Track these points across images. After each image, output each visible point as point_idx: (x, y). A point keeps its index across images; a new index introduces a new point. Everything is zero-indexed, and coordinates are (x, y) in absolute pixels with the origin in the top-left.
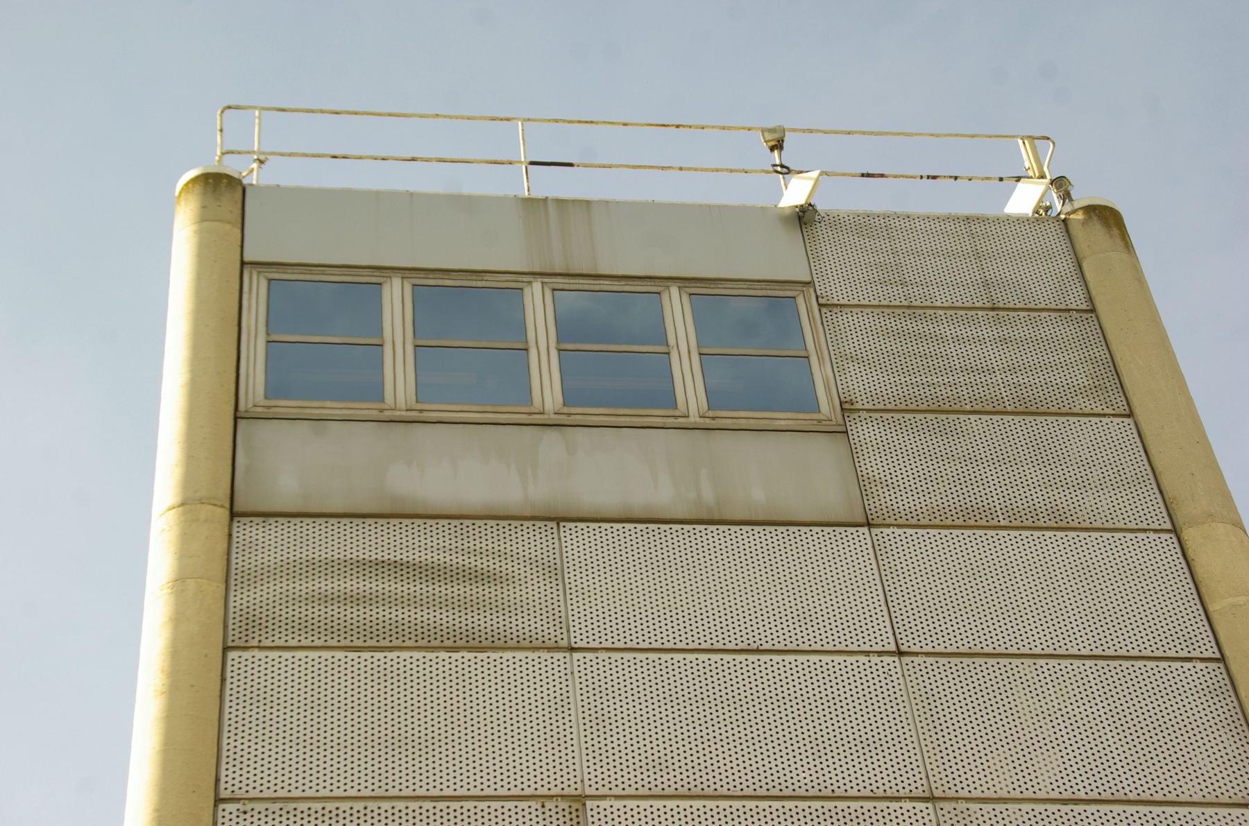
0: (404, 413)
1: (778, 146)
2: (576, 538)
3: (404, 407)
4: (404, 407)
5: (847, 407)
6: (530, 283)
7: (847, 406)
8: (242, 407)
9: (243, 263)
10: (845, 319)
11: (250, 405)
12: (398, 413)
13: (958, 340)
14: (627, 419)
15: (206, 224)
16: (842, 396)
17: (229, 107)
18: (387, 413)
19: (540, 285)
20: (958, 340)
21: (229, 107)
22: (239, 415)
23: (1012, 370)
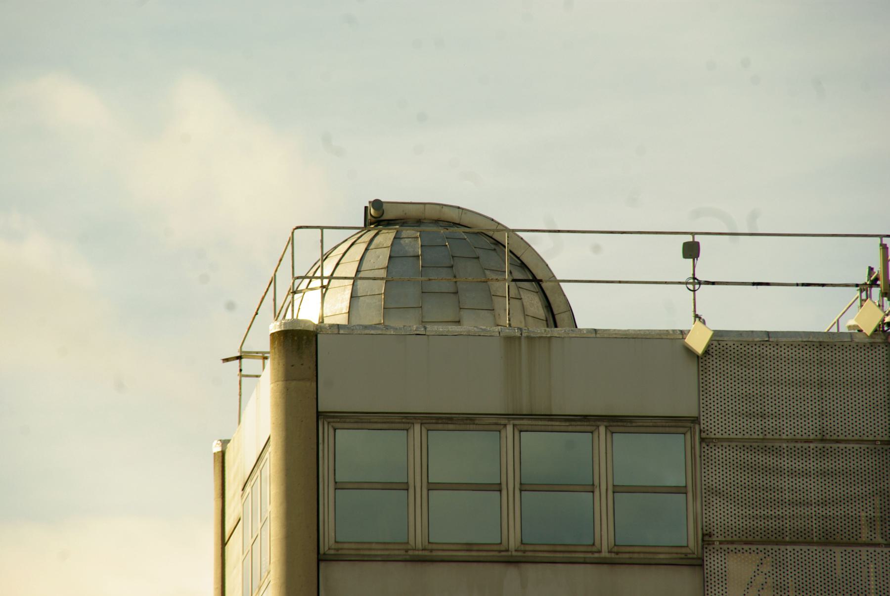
0: (420, 553)
1: (691, 251)
2: (490, 399)
3: (420, 547)
4: (420, 547)
5: (706, 539)
6: (505, 425)
7: (707, 538)
8: (321, 552)
9: (319, 414)
10: (718, 453)
11: (326, 548)
12: (417, 553)
13: (792, 473)
14: (561, 555)
15: (294, 383)
16: (705, 528)
17: (298, 228)
18: (410, 553)
19: (512, 426)
20: (792, 473)
21: (298, 228)
22: (321, 557)
23: (824, 503)
